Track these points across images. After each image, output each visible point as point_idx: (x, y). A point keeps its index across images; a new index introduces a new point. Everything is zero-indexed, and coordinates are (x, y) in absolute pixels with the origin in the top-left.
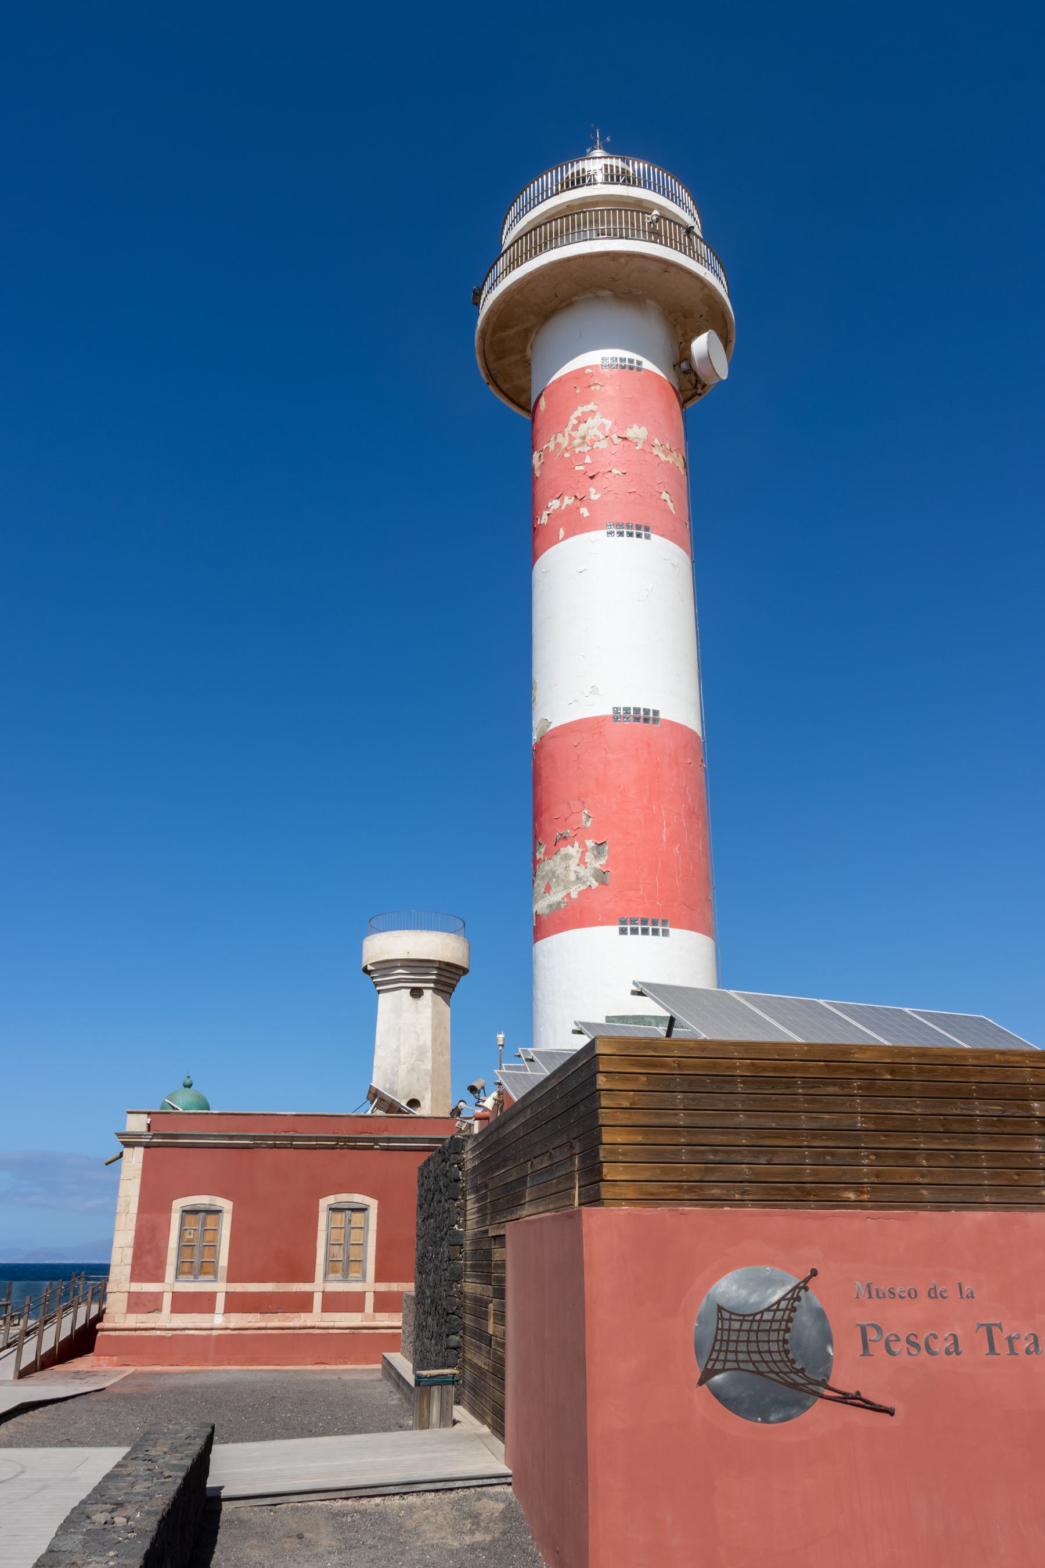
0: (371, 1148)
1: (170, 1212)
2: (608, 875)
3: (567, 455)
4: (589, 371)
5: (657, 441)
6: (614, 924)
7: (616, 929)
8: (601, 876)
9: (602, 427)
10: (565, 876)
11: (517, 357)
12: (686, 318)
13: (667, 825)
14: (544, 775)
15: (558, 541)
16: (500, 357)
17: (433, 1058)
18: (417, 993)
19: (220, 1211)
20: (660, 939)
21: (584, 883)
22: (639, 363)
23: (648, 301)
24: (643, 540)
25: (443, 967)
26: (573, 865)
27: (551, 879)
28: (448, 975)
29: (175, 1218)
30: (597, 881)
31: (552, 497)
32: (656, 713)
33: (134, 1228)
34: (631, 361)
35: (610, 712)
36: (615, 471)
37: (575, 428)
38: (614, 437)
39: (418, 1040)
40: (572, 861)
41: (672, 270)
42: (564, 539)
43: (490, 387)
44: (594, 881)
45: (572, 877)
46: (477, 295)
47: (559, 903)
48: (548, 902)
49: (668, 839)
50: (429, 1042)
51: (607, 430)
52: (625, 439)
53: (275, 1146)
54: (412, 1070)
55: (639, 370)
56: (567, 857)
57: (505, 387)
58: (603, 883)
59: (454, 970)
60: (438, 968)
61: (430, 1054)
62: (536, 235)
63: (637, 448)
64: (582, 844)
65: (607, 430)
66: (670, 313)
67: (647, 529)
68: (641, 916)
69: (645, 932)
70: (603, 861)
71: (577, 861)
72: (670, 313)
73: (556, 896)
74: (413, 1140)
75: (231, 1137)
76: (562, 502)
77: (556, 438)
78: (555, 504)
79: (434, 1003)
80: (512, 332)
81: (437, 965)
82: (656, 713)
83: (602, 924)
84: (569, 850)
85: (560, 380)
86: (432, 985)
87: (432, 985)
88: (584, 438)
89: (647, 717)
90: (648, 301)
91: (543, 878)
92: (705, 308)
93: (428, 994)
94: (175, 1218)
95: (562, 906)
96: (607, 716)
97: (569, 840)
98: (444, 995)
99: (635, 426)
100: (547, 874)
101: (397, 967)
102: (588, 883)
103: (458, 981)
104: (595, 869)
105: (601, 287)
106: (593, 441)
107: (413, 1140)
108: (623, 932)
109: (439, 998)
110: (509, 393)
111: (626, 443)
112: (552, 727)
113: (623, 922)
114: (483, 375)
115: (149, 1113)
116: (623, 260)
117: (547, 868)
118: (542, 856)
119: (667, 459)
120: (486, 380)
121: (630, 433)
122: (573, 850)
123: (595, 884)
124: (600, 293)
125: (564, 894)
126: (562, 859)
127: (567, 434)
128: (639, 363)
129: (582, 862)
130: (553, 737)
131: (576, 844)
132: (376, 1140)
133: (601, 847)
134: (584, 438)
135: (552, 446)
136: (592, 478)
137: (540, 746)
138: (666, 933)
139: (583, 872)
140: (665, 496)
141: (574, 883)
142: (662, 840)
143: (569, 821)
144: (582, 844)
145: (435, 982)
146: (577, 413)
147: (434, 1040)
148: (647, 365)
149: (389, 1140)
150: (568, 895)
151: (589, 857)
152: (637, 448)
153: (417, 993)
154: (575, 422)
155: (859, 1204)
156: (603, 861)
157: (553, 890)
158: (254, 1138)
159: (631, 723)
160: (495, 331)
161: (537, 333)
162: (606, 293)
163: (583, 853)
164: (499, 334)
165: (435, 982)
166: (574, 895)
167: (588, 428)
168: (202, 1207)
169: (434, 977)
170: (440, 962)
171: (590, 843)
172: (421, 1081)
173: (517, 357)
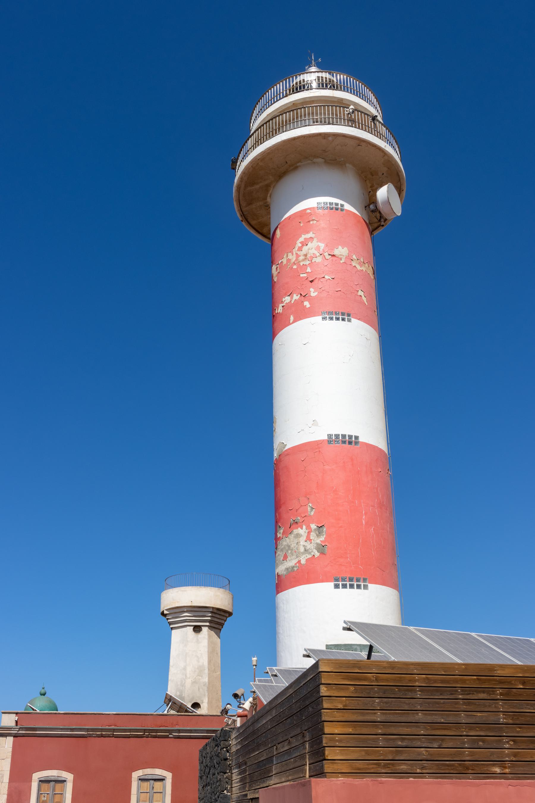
0: (167, 737)
1: (31, 781)
3: (295, 267)
4: (308, 211)
5: (354, 257)
7: (332, 584)
8: (321, 548)
9: (318, 248)
11: (261, 203)
14: (282, 480)
15: (290, 324)
16: (249, 204)
17: (209, 674)
18: (197, 629)
19: (65, 781)
20: (362, 591)
21: (310, 553)
22: (342, 206)
23: (347, 165)
24: (346, 322)
25: (215, 611)
26: (302, 542)
27: (287, 551)
28: (219, 617)
29: (35, 786)
30: (318, 552)
31: (286, 295)
32: (357, 438)
33: (6, 792)
34: (337, 204)
35: (326, 438)
37: (300, 249)
38: (326, 254)
39: (198, 662)
40: (301, 539)
42: (293, 322)
43: (244, 223)
45: (302, 549)
47: (293, 567)
50: (206, 663)
51: (321, 250)
52: (334, 256)
53: (102, 736)
54: (194, 682)
55: (342, 210)
56: (298, 536)
57: (253, 223)
58: (322, 553)
59: (222, 613)
60: (212, 612)
61: (206, 671)
63: (342, 262)
64: (308, 527)
65: (321, 250)
67: (349, 315)
69: (352, 586)
71: (305, 538)
73: (291, 563)
75: (72, 730)
76: (292, 298)
77: (287, 256)
78: (287, 299)
79: (210, 636)
80: (257, 187)
81: (211, 610)
82: (357, 438)
83: (322, 581)
86: (208, 624)
87: (208, 624)
88: (306, 255)
89: (351, 441)
90: (347, 165)
91: (282, 550)
93: (205, 630)
94: (35, 786)
96: (323, 440)
97: (299, 524)
99: (340, 247)
100: (284, 548)
101: (184, 612)
102: (313, 554)
103: (225, 621)
104: (317, 544)
106: (312, 258)
108: (337, 586)
109: (213, 633)
110: (256, 227)
111: (334, 258)
112: (287, 448)
113: (337, 580)
115: (17, 713)
116: (330, 138)
117: (284, 543)
118: (281, 535)
119: (361, 269)
120: (240, 218)
121: (336, 252)
122: (302, 531)
123: (317, 554)
124: (315, 160)
127: (294, 253)
128: (342, 206)
129: (308, 539)
130: (288, 455)
131: (304, 527)
133: (321, 529)
134: (306, 255)
135: (284, 261)
136: (311, 282)
137: (279, 461)
138: (366, 587)
139: (309, 546)
140: (360, 293)
141: (303, 553)
144: (308, 527)
145: (210, 621)
146: (301, 239)
147: (210, 662)
148: (347, 207)
149: (179, 731)
150: (299, 562)
151: (313, 535)
152: (342, 262)
153: (197, 629)
154: (300, 245)
155: (503, 776)
156: (322, 538)
157: (289, 558)
158: (88, 730)
160: (246, 186)
161: (274, 187)
162: (320, 160)
163: (309, 533)
164: (249, 188)
165: (210, 621)
166: (303, 562)
168: (53, 778)
169: (209, 618)
170: (213, 608)
171: (313, 526)
172: (201, 690)
173: (261, 203)
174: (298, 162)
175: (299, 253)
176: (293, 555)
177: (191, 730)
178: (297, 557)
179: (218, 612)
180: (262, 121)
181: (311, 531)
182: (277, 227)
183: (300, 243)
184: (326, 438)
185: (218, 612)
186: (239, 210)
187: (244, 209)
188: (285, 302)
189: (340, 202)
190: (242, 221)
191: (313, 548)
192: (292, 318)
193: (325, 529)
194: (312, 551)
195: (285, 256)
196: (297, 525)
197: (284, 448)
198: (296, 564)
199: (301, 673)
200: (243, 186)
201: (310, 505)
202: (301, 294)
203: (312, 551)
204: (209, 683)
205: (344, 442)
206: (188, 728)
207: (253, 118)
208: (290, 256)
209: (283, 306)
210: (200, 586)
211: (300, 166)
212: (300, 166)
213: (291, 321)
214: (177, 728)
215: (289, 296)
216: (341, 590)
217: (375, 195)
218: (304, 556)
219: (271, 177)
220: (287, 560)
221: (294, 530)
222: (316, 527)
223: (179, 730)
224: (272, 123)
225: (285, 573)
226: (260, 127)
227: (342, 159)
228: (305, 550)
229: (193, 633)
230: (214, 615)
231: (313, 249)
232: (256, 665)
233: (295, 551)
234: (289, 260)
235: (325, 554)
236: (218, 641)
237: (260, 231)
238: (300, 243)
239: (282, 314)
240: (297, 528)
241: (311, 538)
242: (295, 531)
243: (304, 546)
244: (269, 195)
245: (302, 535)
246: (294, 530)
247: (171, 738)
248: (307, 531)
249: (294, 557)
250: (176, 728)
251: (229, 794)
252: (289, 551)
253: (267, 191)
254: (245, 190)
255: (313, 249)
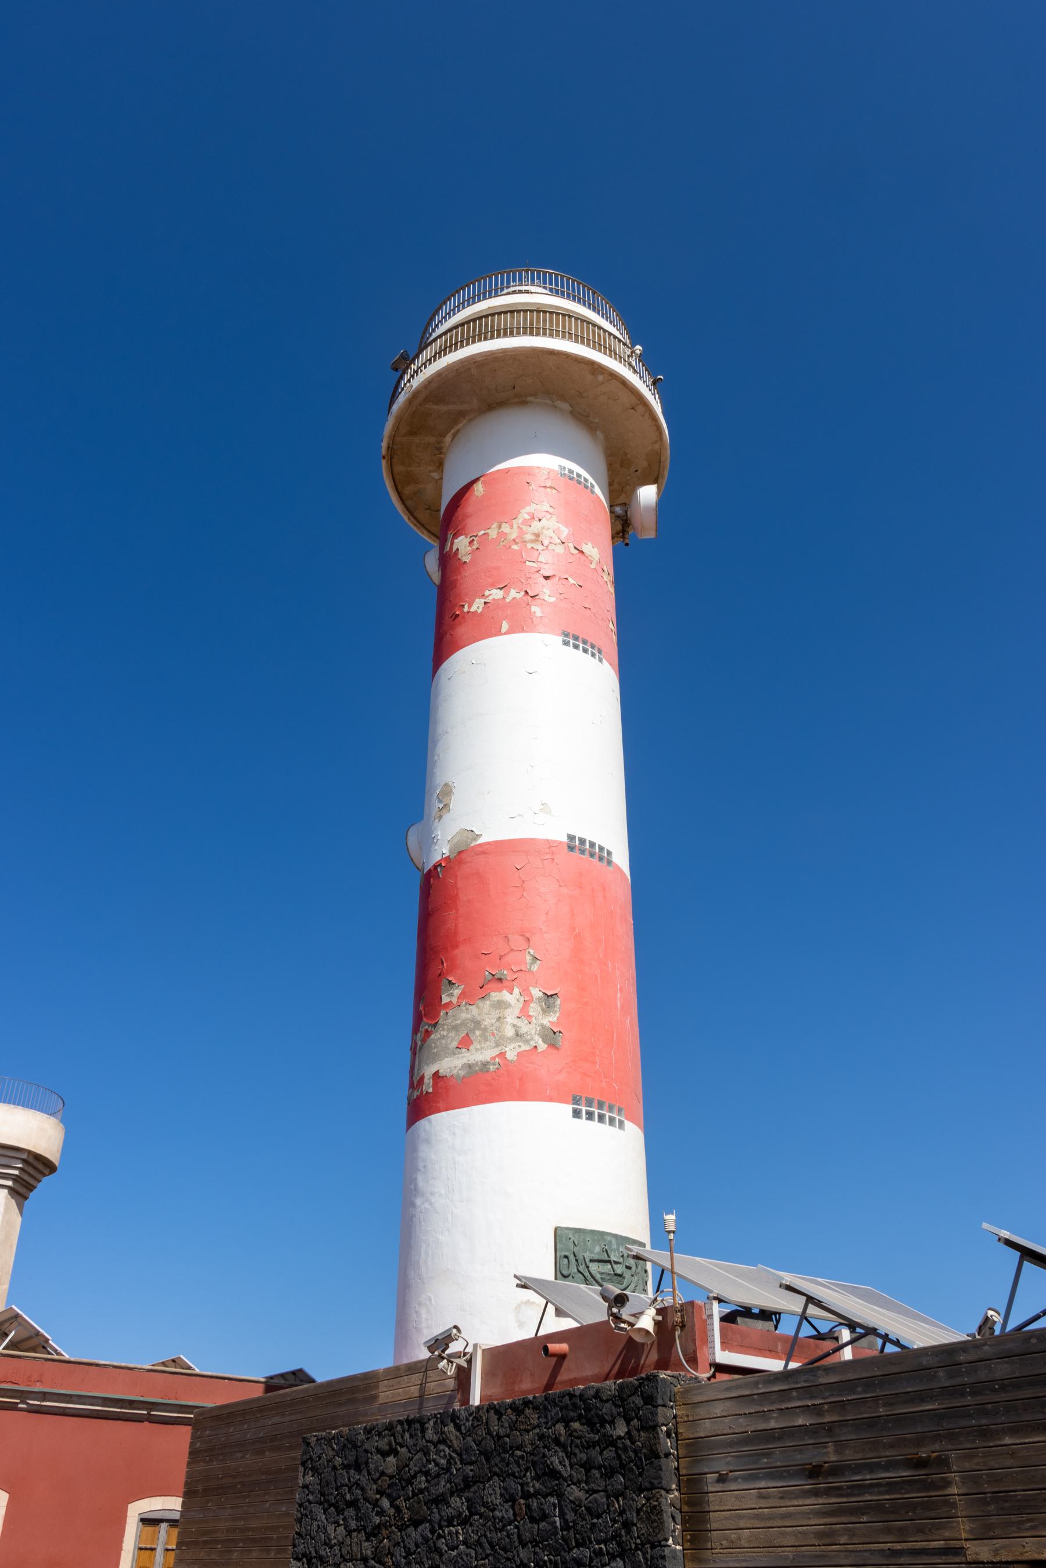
0: (13, 1407)
2: (559, 1036)
3: (515, 547)
6: (567, 1102)
7: (568, 1108)
8: (551, 1036)
10: (498, 1029)
11: (432, 440)
12: (622, 466)
13: (621, 990)
14: (463, 897)
15: (498, 633)
16: (412, 433)
20: (615, 1130)
21: (527, 1042)
23: (598, 433)
25: (31, 1160)
26: (511, 1017)
27: (473, 1031)
30: (544, 1041)
31: (493, 586)
36: (571, 581)
38: (571, 545)
40: (508, 1011)
41: (641, 409)
42: (505, 634)
43: (384, 463)
44: (540, 1042)
45: (510, 1032)
46: (403, 364)
47: (485, 1064)
48: (465, 1061)
49: (622, 1006)
52: (582, 552)
56: (501, 1005)
57: (399, 468)
58: (553, 1046)
59: (41, 1167)
60: (24, 1161)
62: (469, 328)
64: (525, 992)
66: (611, 455)
68: (597, 1098)
70: (553, 1018)
71: (517, 1013)
72: (611, 455)
73: (481, 1054)
74: (81, 1399)
76: (508, 594)
77: (500, 527)
78: (496, 594)
80: (444, 408)
81: (24, 1156)
83: (550, 1099)
84: (505, 995)
85: (507, 471)
86: (10, 1183)
87: (10, 1183)
90: (598, 433)
91: (455, 1028)
92: (645, 464)
95: (492, 1068)
96: (561, 842)
97: (505, 983)
100: (463, 1024)
102: (533, 1044)
103: (39, 1181)
104: (543, 1026)
105: (563, 398)
107: (81, 1399)
108: (577, 1114)
109: (13, 1201)
110: (397, 478)
111: (581, 555)
112: (480, 841)
114: (384, 444)
116: (600, 378)
117: (464, 1015)
118: (454, 1000)
120: (384, 451)
122: (512, 998)
123: (542, 1046)
124: (559, 403)
125: (496, 1052)
126: (491, 1006)
127: (515, 526)
129: (524, 1013)
130: (484, 853)
131: (516, 991)
132: (23, 1395)
133: (551, 1000)
134: (537, 535)
135: (493, 533)
136: (547, 578)
137: (450, 864)
139: (524, 1028)
141: (511, 1040)
142: (616, 1007)
143: (504, 960)
145: (15, 1179)
148: (597, 490)
149: (44, 1396)
150: (502, 1055)
151: (534, 1009)
154: (527, 517)
156: (553, 1018)
157: (476, 1045)
159: (595, 860)
160: (426, 400)
161: (470, 420)
162: (566, 406)
164: (430, 406)
165: (15, 1179)
166: (511, 1056)
167: (543, 528)
169: (16, 1172)
170: (29, 1152)
171: (536, 993)
173: (432, 440)
174: (532, 395)
175: (524, 528)
176: (486, 1040)
177: (71, 1396)
178: (498, 1045)
181: (532, 1000)
182: (477, 480)
183: (528, 514)
184: (565, 839)
186: (390, 437)
187: (398, 439)
188: (491, 598)
189: (591, 480)
190: (384, 457)
191: (533, 1032)
192: (505, 626)
193: (558, 1002)
194: (532, 1039)
195: (494, 526)
196: (499, 985)
197: (475, 840)
198: (493, 1058)
200: (422, 397)
201: (532, 952)
202: (526, 592)
203: (532, 1039)
205: (592, 855)
206: (62, 1392)
208: (505, 528)
209: (485, 603)
210: (14, 1104)
211: (531, 402)
212: (531, 402)
213: (503, 630)
214: (39, 1388)
215: (501, 589)
216: (583, 1121)
217: (634, 491)
218: (516, 1045)
219: (475, 401)
220: (471, 1048)
221: (493, 994)
222: (541, 994)
223: (45, 1393)
224: (469, 328)
225: (462, 1073)
226: (462, 325)
227: (597, 421)
228: (517, 1035)
231: (551, 531)
232: (674, 1232)
233: (493, 1034)
234: (502, 535)
235: (557, 1049)
236: (19, 1220)
237: (399, 487)
238: (528, 514)
239: (481, 614)
240: (500, 991)
241: (531, 1014)
242: (495, 996)
243: (514, 1026)
244: (453, 431)
245: (510, 1005)
246: (493, 994)
247: (21, 1410)
248: (522, 999)
249: (493, 1044)
250: (36, 1389)
251: (678, 1547)
252: (478, 1033)
253: (455, 422)
254: (420, 405)
255: (551, 531)
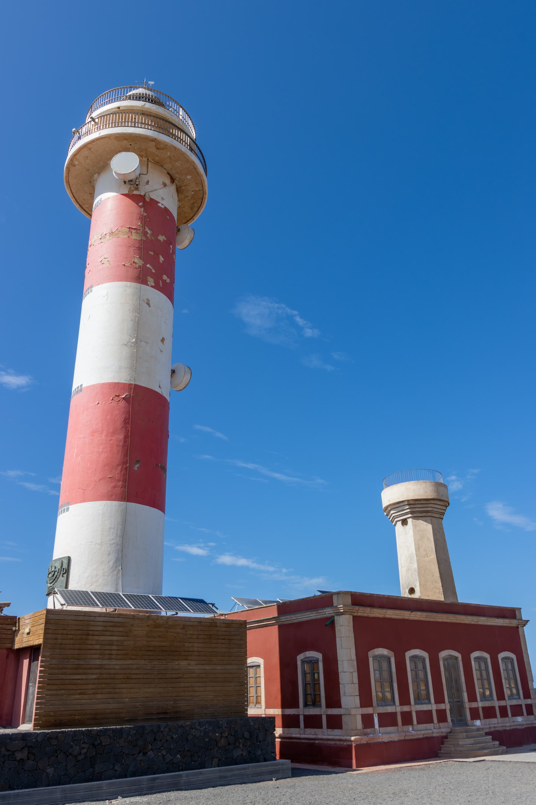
18: (404, 522)
25: (413, 502)
28: (420, 506)
54: (408, 570)
59: (424, 502)
60: (408, 505)
61: (415, 558)
79: (415, 526)
81: (406, 503)
86: (410, 515)
87: (410, 515)
93: (410, 521)
98: (424, 518)
145: (411, 513)
147: (418, 548)
153: (404, 522)
169: (408, 510)
170: (408, 501)
172: (413, 576)
179: (416, 502)
180: (103, 112)
185: (416, 502)
199: (60, 504)
204: (419, 568)
207: (70, 147)
229: (402, 526)
230: (413, 506)
